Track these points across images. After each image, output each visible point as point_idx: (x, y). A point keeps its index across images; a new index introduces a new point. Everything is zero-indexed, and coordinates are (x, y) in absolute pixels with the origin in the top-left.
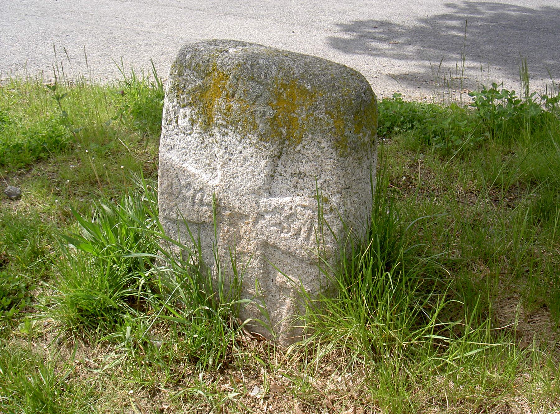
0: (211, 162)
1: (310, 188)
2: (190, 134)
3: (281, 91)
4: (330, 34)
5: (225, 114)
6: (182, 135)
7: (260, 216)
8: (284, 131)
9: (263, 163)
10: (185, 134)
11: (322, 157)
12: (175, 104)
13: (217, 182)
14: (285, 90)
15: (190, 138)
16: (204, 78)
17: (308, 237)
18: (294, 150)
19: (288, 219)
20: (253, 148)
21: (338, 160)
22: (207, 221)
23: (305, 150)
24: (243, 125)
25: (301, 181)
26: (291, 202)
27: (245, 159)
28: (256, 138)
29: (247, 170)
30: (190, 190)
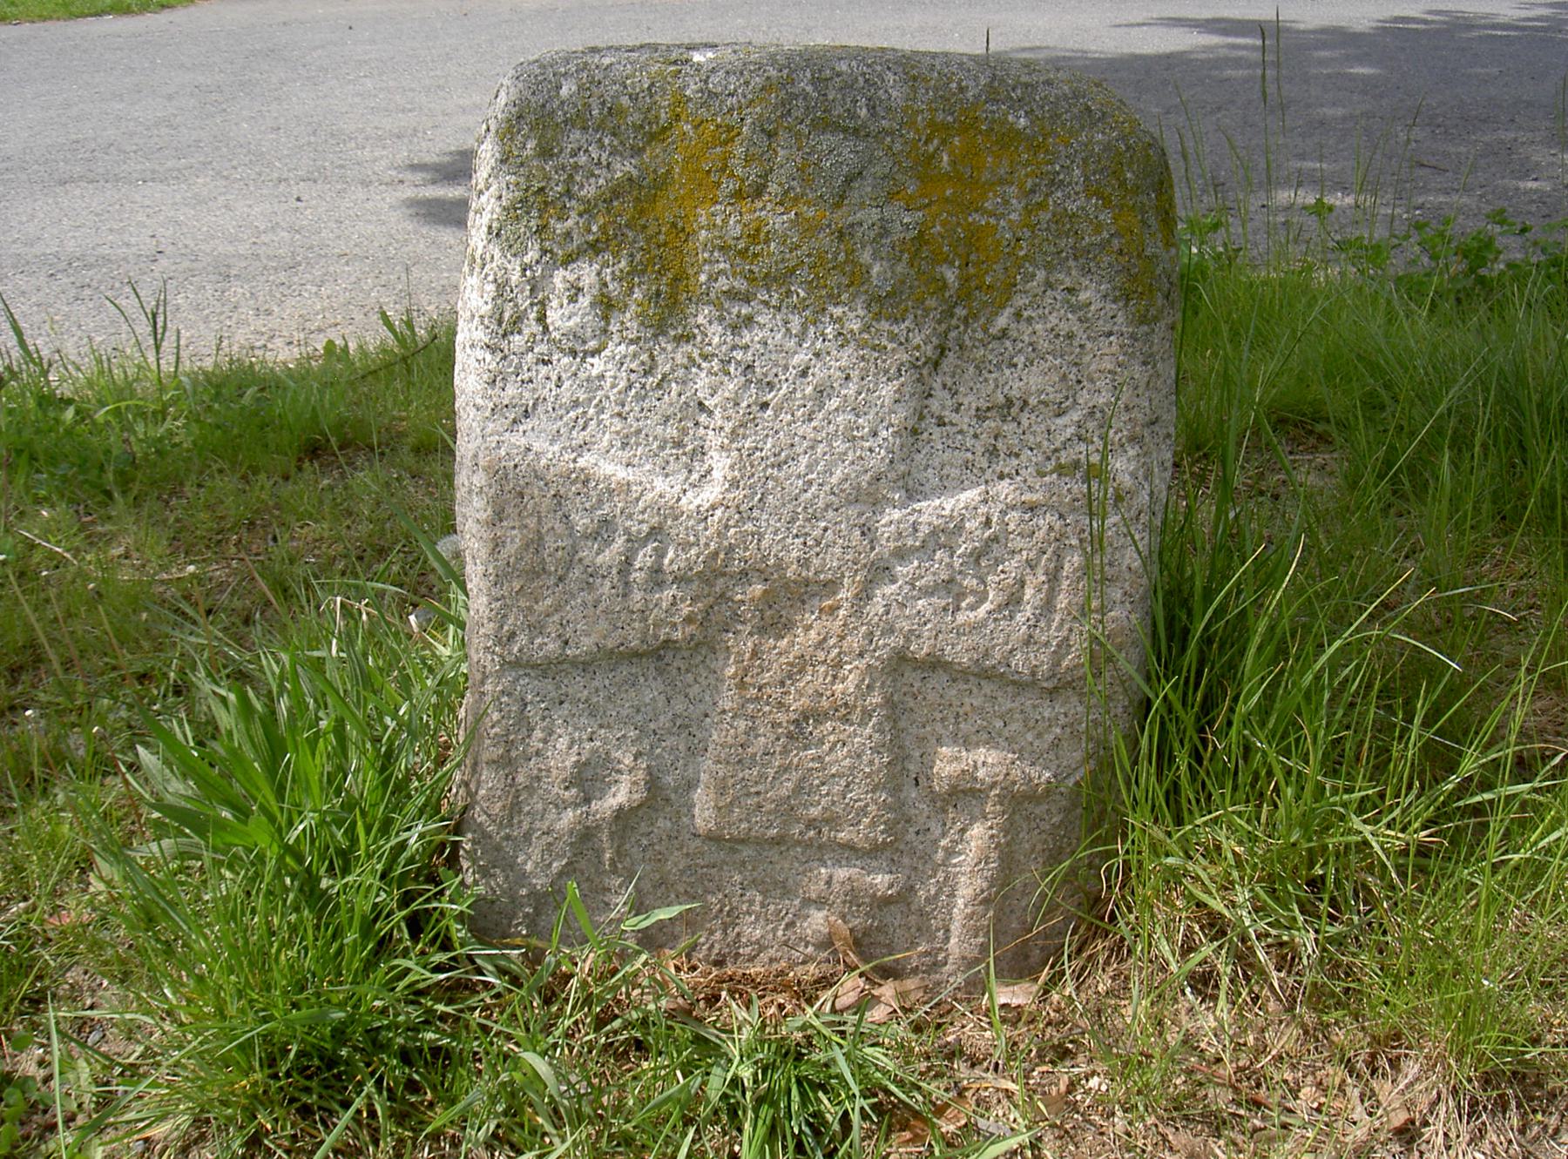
0: (684, 432)
1: (1039, 445)
2: (596, 352)
3: (931, 149)
4: (409, 192)
5: (743, 253)
6: (566, 360)
7: (880, 572)
8: (951, 275)
9: (887, 391)
10: (574, 353)
11: (1081, 338)
12: (532, 255)
13: (711, 493)
14: (943, 142)
15: (597, 365)
16: (641, 151)
17: (1048, 606)
18: (985, 331)
19: (977, 561)
20: (849, 350)
21: (1133, 337)
22: (677, 635)
23: (1023, 326)
24: (816, 277)
25: (1009, 427)
26: (985, 501)
27: (821, 393)
28: (861, 312)
29: (832, 428)
30: (608, 542)
